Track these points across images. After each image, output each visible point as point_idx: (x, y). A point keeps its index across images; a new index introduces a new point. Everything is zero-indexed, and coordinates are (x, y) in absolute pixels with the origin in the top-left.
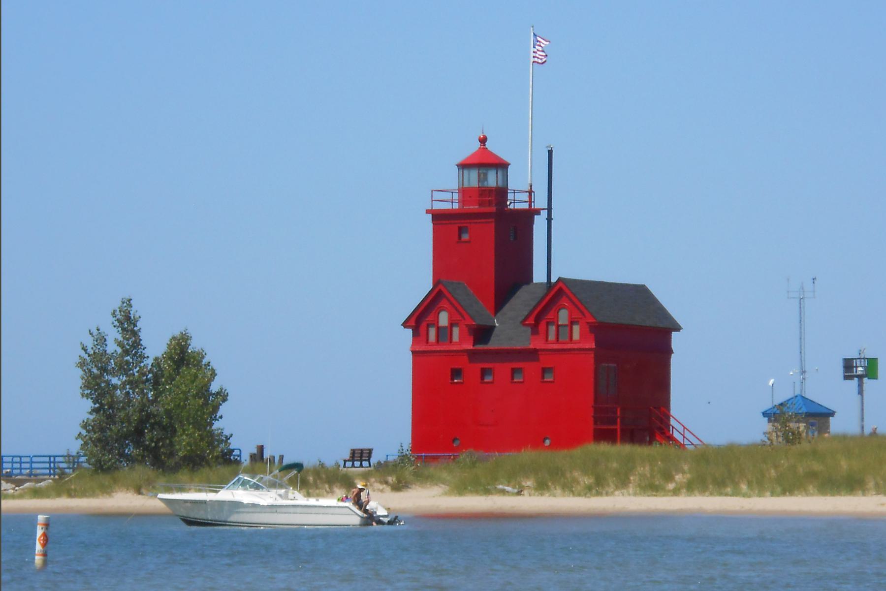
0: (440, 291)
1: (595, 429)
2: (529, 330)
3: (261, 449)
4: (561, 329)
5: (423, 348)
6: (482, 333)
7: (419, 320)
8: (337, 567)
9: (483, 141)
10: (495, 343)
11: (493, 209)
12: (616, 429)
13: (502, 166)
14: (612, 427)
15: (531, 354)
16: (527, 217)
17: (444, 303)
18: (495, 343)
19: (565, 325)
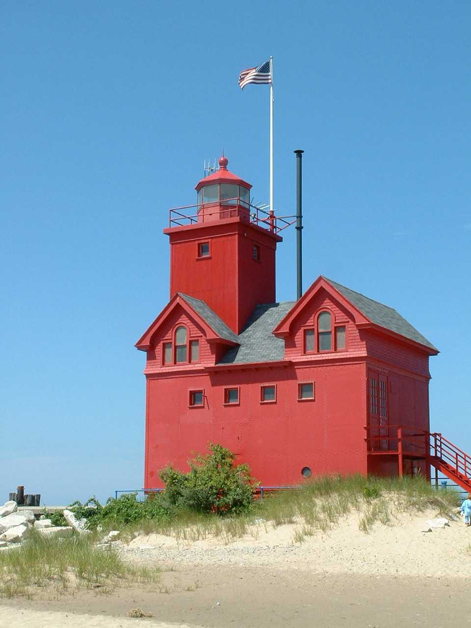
0: (178, 305)
1: (369, 456)
2: (144, 354)
3: (21, 489)
4: (178, 350)
5: (158, 369)
6: (225, 350)
7: (154, 341)
8: (120, 575)
9: (224, 164)
10: (240, 359)
11: (237, 219)
12: (398, 455)
13: (245, 187)
14: (396, 453)
15: (286, 370)
16: (270, 240)
17: (183, 319)
18: (240, 359)
19: (184, 346)
